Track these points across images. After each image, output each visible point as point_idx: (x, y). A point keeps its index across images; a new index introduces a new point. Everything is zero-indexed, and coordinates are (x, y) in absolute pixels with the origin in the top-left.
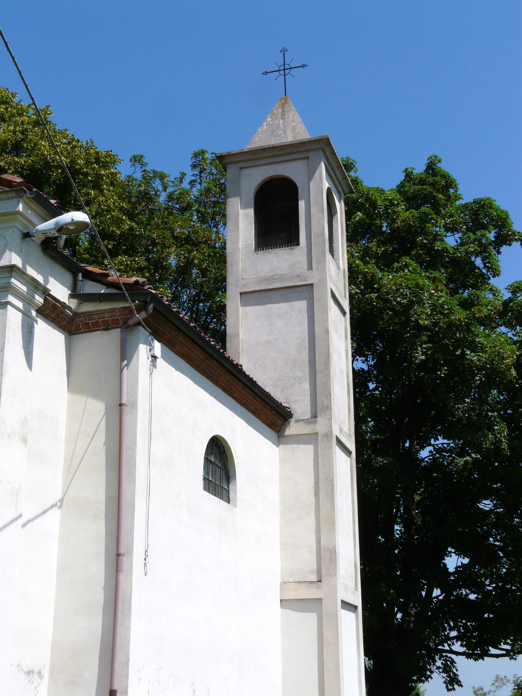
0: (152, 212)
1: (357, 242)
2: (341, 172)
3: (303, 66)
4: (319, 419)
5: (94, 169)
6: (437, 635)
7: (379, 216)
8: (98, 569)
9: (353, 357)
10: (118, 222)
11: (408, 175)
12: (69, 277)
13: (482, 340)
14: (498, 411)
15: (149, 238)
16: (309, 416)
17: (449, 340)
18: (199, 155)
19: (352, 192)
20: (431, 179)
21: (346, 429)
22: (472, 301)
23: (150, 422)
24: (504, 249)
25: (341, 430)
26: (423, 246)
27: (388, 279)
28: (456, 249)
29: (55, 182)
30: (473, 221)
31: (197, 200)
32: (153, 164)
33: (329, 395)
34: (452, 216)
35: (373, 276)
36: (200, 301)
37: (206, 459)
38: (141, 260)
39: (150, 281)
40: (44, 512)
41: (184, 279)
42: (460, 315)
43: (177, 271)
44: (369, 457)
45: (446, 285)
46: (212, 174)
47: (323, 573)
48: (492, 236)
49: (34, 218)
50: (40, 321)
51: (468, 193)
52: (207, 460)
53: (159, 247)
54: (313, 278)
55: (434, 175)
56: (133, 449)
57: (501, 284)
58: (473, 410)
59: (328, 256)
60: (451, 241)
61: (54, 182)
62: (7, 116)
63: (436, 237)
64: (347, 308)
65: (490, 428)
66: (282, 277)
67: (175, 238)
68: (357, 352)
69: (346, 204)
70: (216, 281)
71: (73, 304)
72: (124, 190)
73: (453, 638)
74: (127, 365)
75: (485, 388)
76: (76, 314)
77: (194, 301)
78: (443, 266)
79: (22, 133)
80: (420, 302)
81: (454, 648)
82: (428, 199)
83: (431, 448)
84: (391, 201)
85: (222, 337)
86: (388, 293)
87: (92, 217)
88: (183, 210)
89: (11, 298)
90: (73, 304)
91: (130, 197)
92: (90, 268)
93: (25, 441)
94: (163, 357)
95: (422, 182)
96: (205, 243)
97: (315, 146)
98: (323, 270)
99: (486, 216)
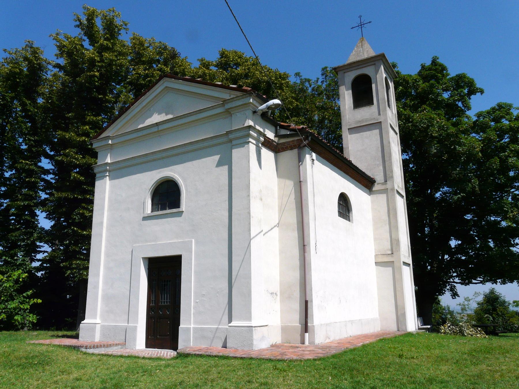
0: (305, 97)
1: (400, 101)
2: (390, 68)
3: (370, 22)
4: (388, 182)
5: (279, 81)
6: (447, 275)
7: (410, 87)
8: (296, 252)
9: (402, 153)
10: (291, 103)
11: (423, 67)
12: (273, 128)
13: (463, 140)
14: (473, 173)
15: (305, 108)
16: (383, 181)
17: (447, 142)
18: (324, 69)
19: (396, 78)
20: (434, 68)
21: (401, 186)
22: (458, 123)
23: (314, 188)
24: (472, 97)
25: (398, 187)
26: (432, 99)
27: (416, 116)
28: (448, 99)
29: (264, 89)
30: (456, 85)
31: (325, 90)
32: (304, 76)
33: (392, 171)
34: (445, 84)
35: (409, 115)
36: (329, 134)
37: (338, 203)
38: (302, 119)
39: (309, 127)
40: (272, 229)
41: (322, 125)
42: (452, 130)
43: (319, 122)
44: (412, 198)
45: (445, 117)
46: (331, 77)
47: (394, 250)
48: (466, 91)
49: (257, 105)
50: (263, 148)
51: (453, 72)
52: (339, 204)
53: (310, 112)
54: (381, 119)
55: (436, 65)
56: (307, 200)
57: (472, 114)
58: (461, 173)
59: (388, 108)
60: (446, 95)
61: (263, 89)
62: (241, 63)
63: (439, 95)
64: (398, 132)
65: (470, 181)
66: (366, 120)
67: (316, 107)
68: (403, 151)
69: (394, 84)
70: (336, 125)
71: (276, 140)
72: (292, 88)
73: (455, 276)
74: (302, 164)
75: (467, 162)
76: (278, 144)
77: (327, 135)
78: (443, 108)
79: (248, 69)
80: (432, 125)
81: (455, 281)
82: (433, 77)
83: (441, 192)
84: (415, 80)
85: (341, 149)
86: (417, 123)
87: (281, 100)
88: (319, 95)
89: (250, 140)
90: (276, 140)
91: (295, 91)
92: (282, 124)
93: (261, 199)
94: (317, 159)
95: (430, 69)
96: (330, 108)
97: (378, 58)
98: (386, 115)
99: (462, 82)
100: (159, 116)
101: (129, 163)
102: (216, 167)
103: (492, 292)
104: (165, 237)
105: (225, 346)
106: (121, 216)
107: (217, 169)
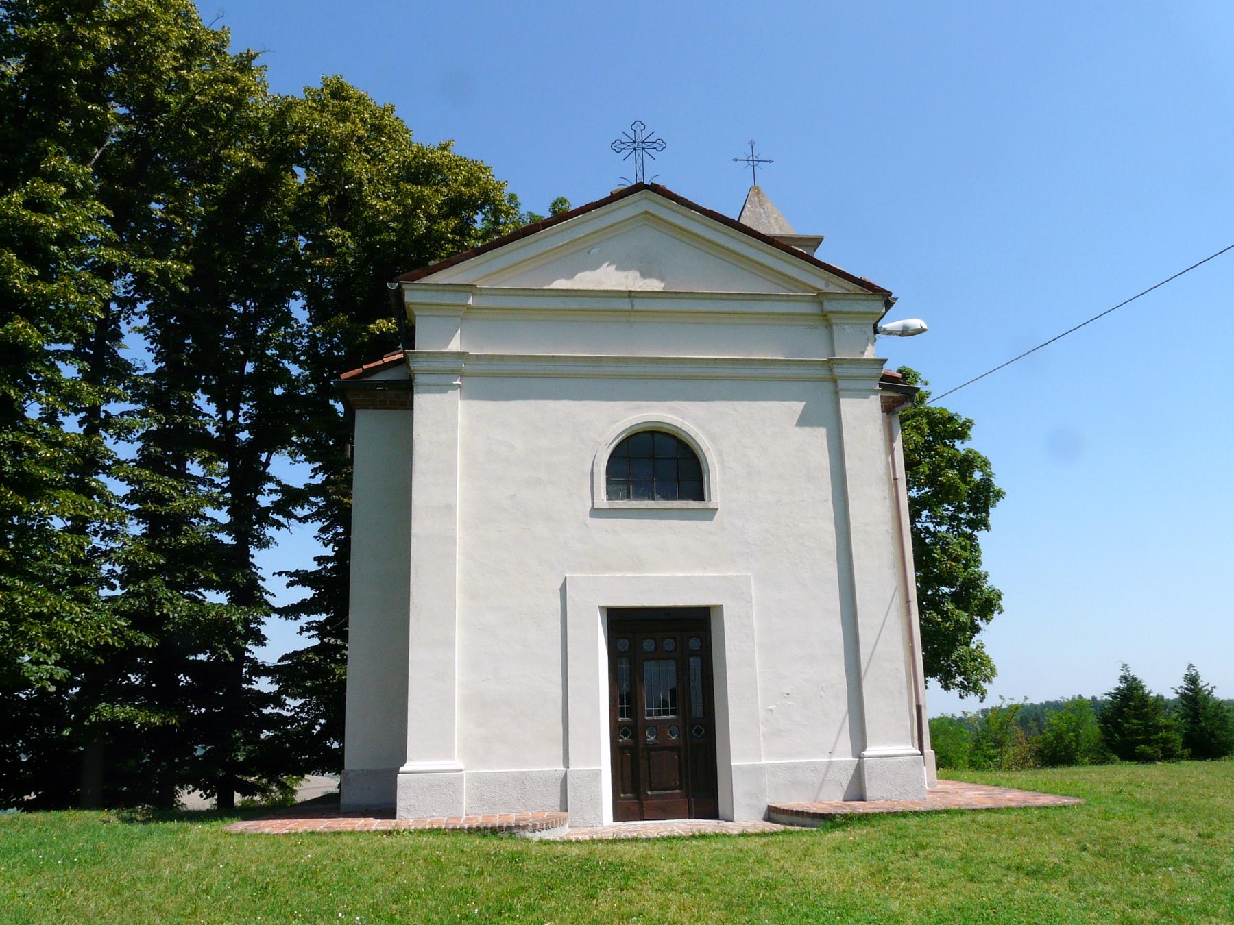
3: (770, 161)
100: (621, 274)
104: (660, 562)
105: (857, 793)
106: (513, 497)
107: (798, 429)
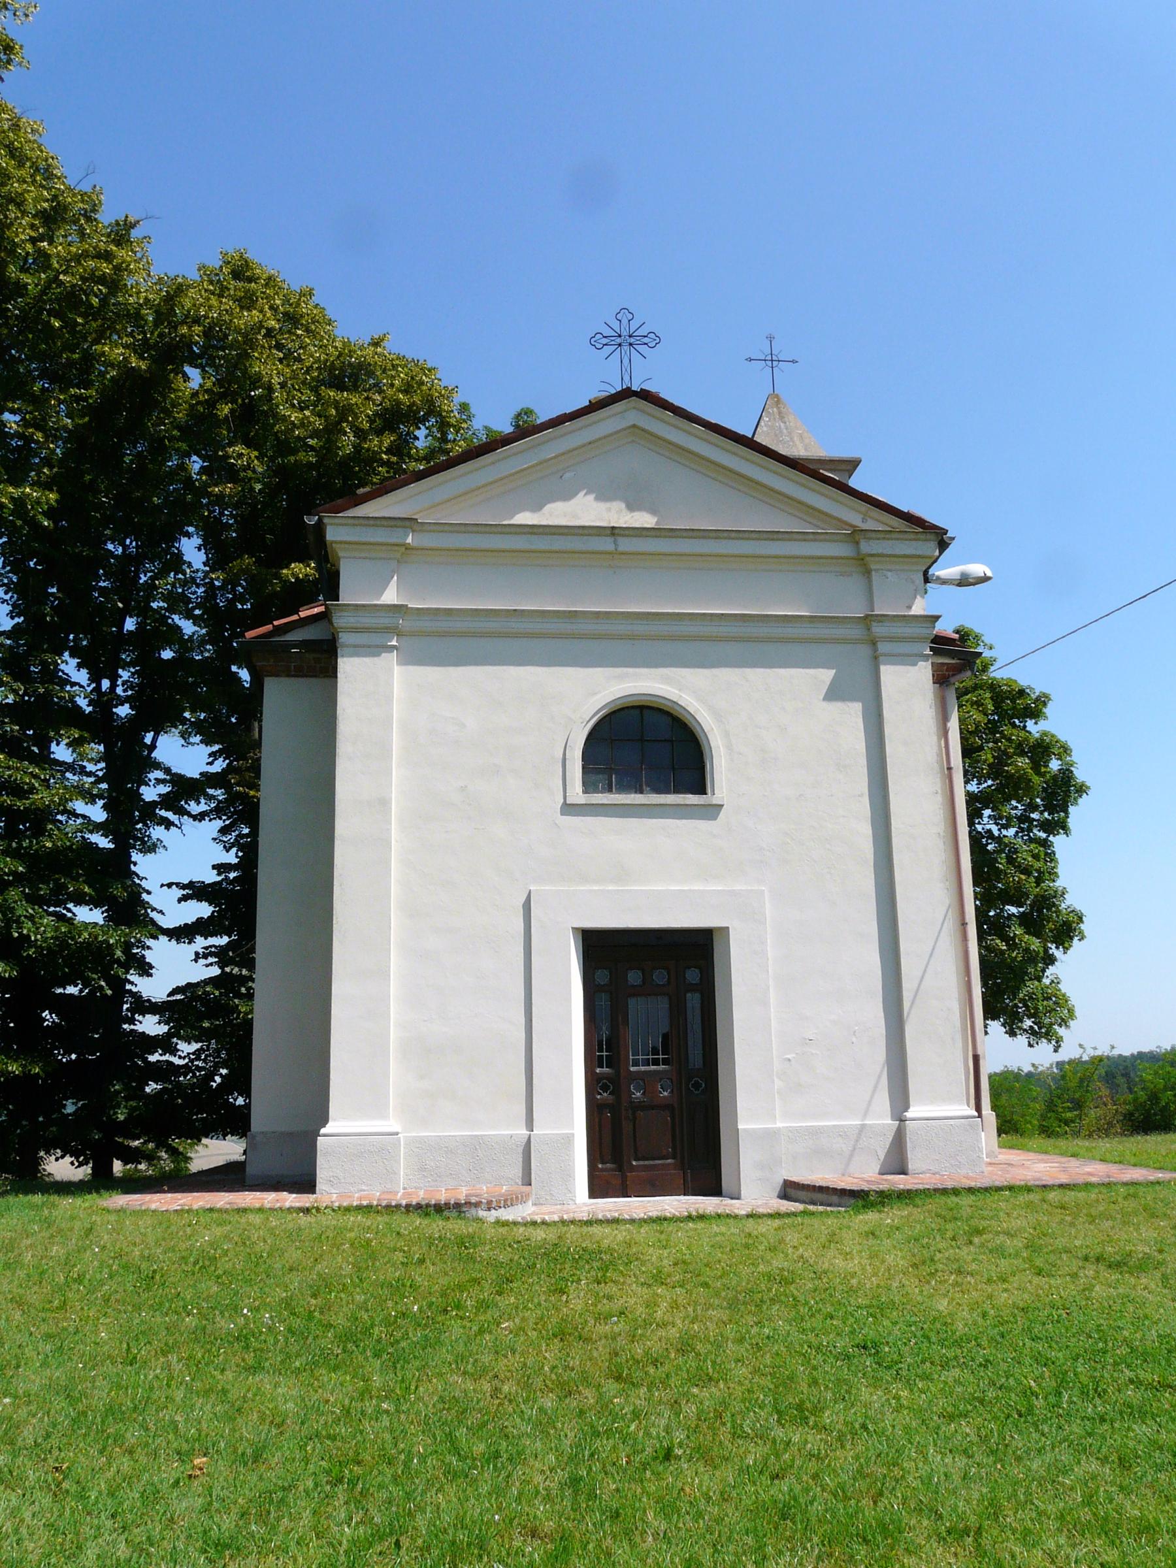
3: (794, 362)
100: (602, 506)
101: (493, 625)
102: (824, 699)
103: (1043, 1033)
107: (825, 704)
